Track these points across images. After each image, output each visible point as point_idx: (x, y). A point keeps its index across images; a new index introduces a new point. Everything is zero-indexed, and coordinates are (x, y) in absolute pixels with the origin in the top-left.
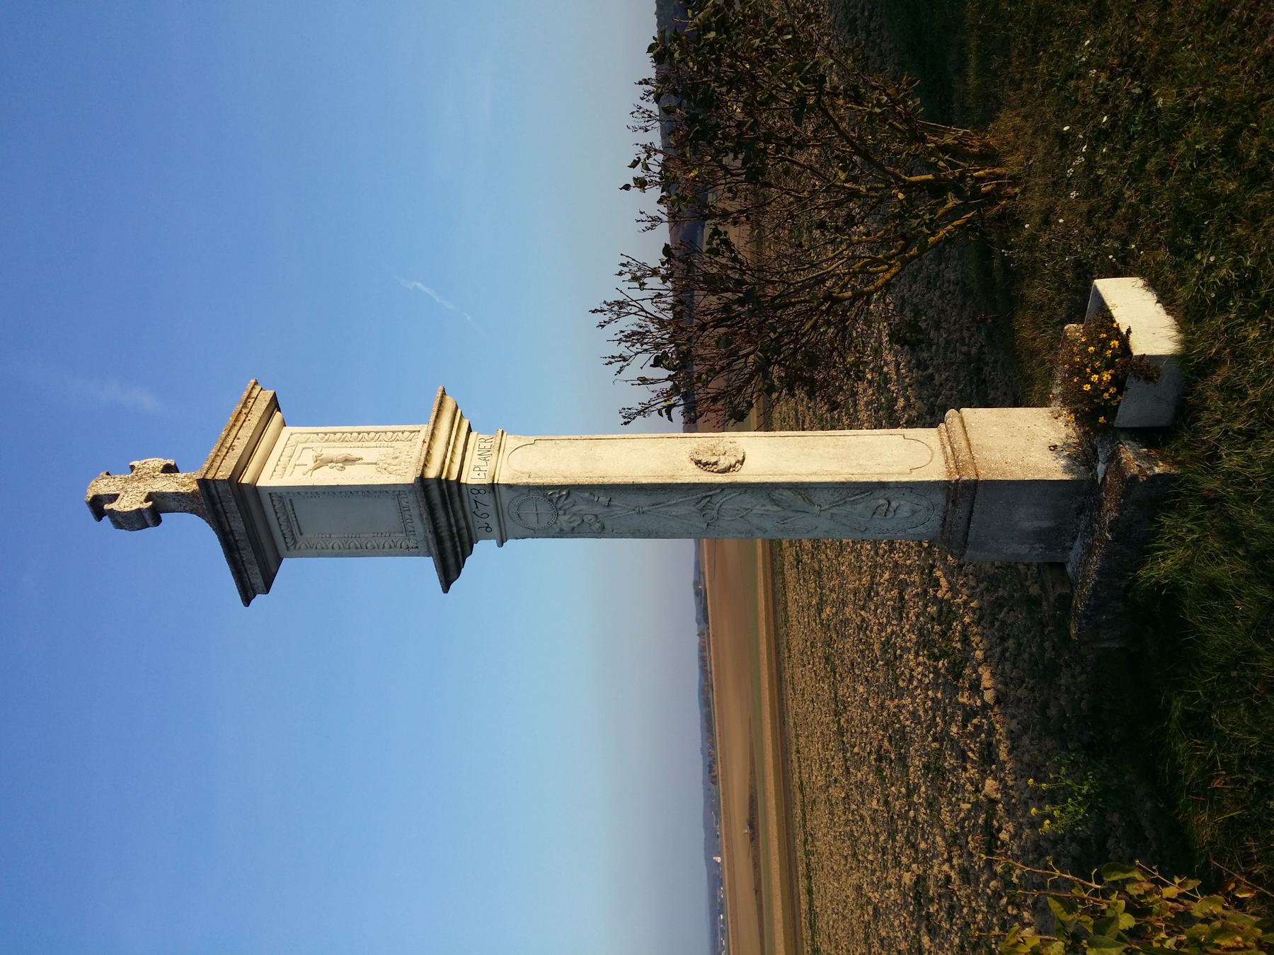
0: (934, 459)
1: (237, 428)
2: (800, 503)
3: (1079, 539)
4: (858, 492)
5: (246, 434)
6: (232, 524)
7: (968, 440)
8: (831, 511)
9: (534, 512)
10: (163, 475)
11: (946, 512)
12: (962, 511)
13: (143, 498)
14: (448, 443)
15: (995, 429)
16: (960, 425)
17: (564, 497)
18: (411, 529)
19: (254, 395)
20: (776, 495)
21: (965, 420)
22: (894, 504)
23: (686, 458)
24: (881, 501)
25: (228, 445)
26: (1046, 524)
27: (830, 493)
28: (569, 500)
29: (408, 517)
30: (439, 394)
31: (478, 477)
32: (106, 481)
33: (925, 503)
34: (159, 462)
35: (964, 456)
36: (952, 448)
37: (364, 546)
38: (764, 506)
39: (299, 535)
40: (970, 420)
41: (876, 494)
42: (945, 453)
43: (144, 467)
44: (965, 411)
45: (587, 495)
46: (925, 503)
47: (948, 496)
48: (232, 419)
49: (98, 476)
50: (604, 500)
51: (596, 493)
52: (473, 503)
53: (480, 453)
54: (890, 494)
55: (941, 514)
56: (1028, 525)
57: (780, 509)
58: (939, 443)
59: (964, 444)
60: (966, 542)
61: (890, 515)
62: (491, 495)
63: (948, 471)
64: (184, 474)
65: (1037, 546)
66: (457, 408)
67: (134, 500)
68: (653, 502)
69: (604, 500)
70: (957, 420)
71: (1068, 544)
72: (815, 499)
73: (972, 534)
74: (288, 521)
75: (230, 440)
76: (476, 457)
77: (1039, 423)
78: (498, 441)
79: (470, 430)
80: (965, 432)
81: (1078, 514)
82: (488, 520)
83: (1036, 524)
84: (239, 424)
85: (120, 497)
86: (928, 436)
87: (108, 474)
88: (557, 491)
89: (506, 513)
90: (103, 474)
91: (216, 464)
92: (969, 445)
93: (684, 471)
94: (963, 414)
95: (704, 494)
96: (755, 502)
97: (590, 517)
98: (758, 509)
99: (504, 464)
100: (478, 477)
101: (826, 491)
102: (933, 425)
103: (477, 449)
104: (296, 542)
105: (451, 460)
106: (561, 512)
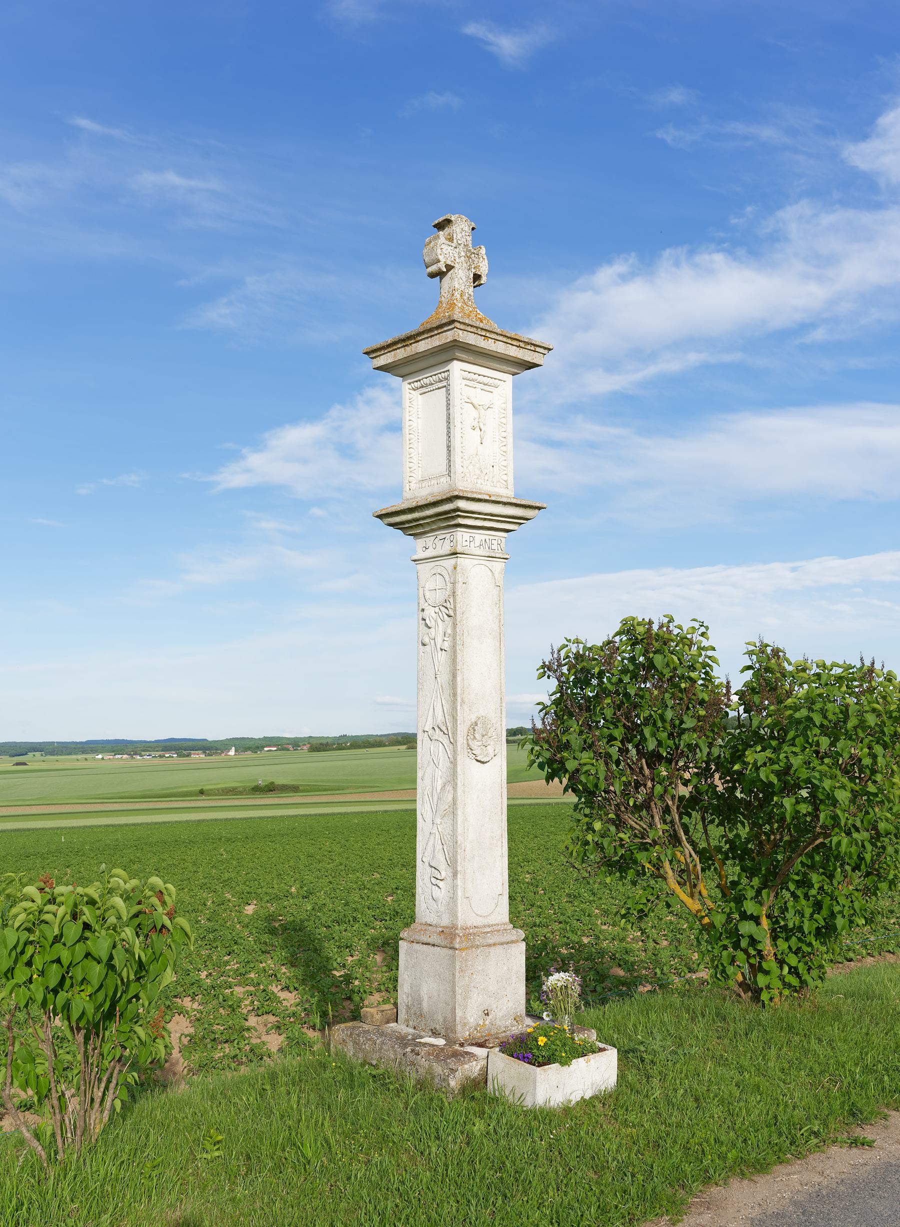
0: (478, 917)
1: (505, 339)
2: (443, 807)
3: (414, 1031)
4: (451, 855)
5: (500, 348)
6: (423, 342)
7: (494, 945)
8: (437, 833)
9: (437, 587)
10: (472, 276)
11: (436, 926)
12: (434, 939)
13: (450, 263)
14: (492, 515)
15: (505, 968)
16: (509, 940)
17: (447, 613)
18: (424, 485)
19: (538, 349)
20: (449, 788)
21: (513, 945)
22: (441, 884)
23: (482, 713)
24: (444, 874)
25: (488, 335)
26: (425, 1005)
27: (450, 832)
28: (446, 616)
29: (424, 485)
30: (538, 505)
31: (464, 540)
32: (466, 229)
33: (442, 909)
34: (484, 268)
35: (478, 941)
36: (488, 932)
37: (411, 446)
38: (441, 778)
39: (420, 392)
40: (513, 949)
41: (450, 870)
42: (485, 926)
43: (479, 258)
44: (523, 946)
45: (449, 631)
46: (442, 909)
47: (447, 927)
48: (513, 335)
49: (471, 221)
50: (446, 646)
51: (451, 638)
52: (444, 536)
53: (487, 541)
54: (449, 880)
55: (434, 923)
56: (424, 991)
57: (439, 791)
58: (494, 923)
59: (491, 942)
60: (413, 942)
61: (433, 880)
62: (449, 552)
63: (467, 928)
64: (472, 294)
65: (410, 998)
66: (527, 519)
67: (447, 256)
68: (444, 686)
69: (446, 646)
70: (514, 938)
71: (411, 1023)
72: (446, 819)
73: (416, 946)
74: (427, 385)
75: (493, 336)
76: (483, 537)
77: (510, 1004)
78: (497, 555)
79: (508, 531)
80: (502, 944)
81: (432, 1030)
82: (431, 549)
83: (426, 998)
84: (509, 341)
85: (450, 243)
86: (502, 913)
87: (473, 229)
88: (452, 607)
89: (437, 563)
90: (473, 225)
91: (469, 329)
92: (490, 945)
93: (468, 711)
94: (520, 944)
95: (449, 728)
96: (443, 770)
97: (433, 634)
98: (439, 773)
99: (476, 562)
100: (464, 540)
101: (451, 828)
102: (511, 921)
103: (491, 538)
104: (414, 390)
105: (477, 518)
106: (437, 610)
